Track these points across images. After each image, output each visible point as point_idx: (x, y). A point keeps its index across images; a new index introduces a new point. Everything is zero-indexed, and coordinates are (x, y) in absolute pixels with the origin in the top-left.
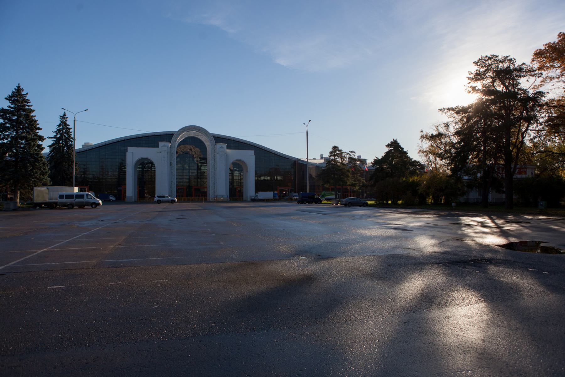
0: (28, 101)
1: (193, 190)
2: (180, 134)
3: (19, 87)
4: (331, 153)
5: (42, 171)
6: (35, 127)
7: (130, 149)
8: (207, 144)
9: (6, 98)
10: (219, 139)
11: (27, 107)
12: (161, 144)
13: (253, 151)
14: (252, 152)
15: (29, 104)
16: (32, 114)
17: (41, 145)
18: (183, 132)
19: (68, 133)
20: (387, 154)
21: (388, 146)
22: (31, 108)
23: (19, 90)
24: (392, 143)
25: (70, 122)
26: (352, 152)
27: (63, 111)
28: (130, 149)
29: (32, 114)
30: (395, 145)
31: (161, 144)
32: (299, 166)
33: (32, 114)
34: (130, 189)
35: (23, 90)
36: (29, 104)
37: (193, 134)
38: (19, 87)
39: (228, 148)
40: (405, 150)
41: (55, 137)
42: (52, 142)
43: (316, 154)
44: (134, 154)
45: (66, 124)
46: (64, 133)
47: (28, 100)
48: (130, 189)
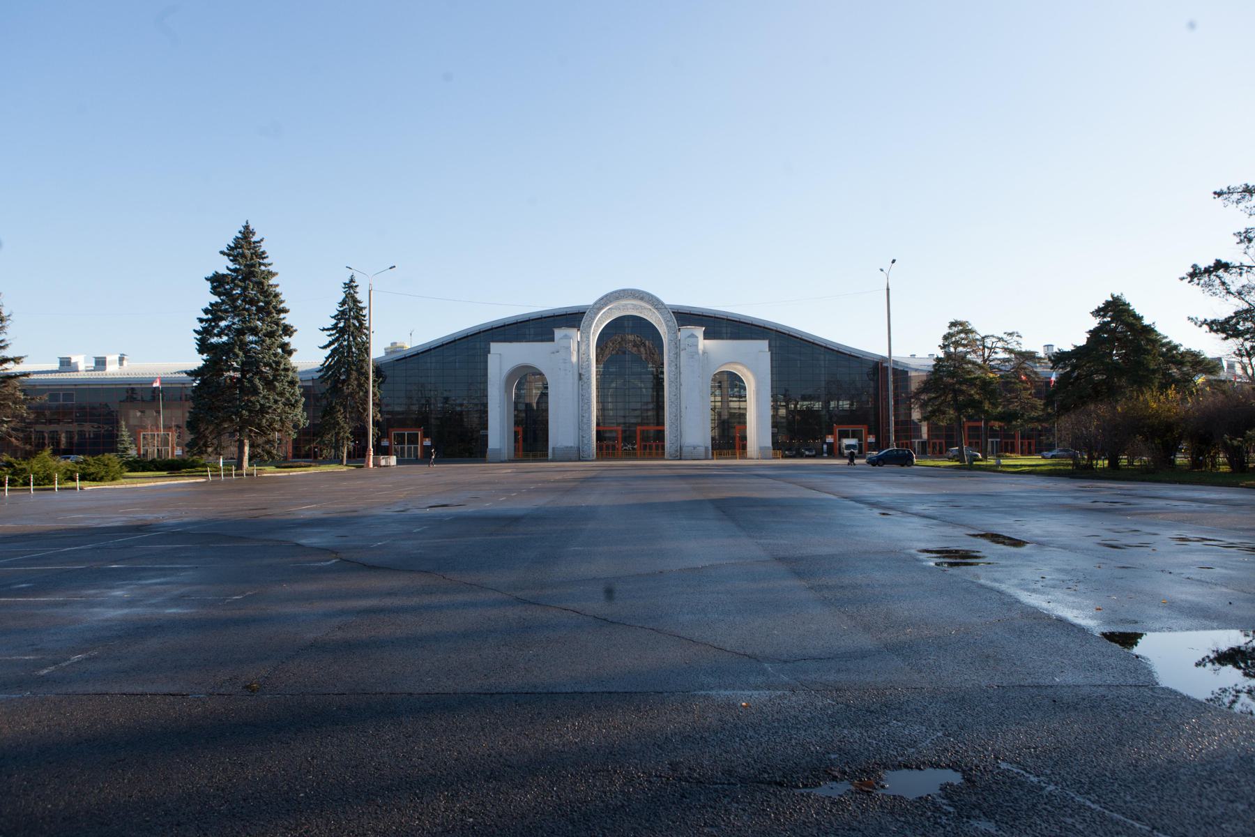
0: (262, 255)
1: (634, 427)
2: (600, 309)
3: (247, 227)
4: (946, 338)
5: (288, 399)
6: (275, 307)
7: (495, 347)
8: (663, 330)
9: (222, 253)
10: (685, 317)
11: (263, 268)
12: (559, 333)
13: (766, 342)
14: (761, 347)
15: (265, 261)
16: (272, 281)
17: (287, 344)
18: (606, 305)
19: (359, 317)
20: (1094, 334)
21: (1097, 313)
22: (270, 268)
23: (247, 232)
24: (1108, 304)
25: (361, 295)
26: (1011, 334)
27: (350, 273)
28: (495, 347)
29: (271, 282)
30: (1116, 309)
31: (559, 333)
32: (879, 373)
33: (272, 281)
34: (498, 431)
35: (254, 234)
36: (265, 261)
37: (630, 308)
38: (247, 227)
39: (707, 336)
40: (1146, 322)
41: (335, 327)
42: (330, 339)
43: (917, 346)
44: (503, 359)
45: (356, 301)
46: (350, 323)
47: (263, 253)
48: (498, 431)
